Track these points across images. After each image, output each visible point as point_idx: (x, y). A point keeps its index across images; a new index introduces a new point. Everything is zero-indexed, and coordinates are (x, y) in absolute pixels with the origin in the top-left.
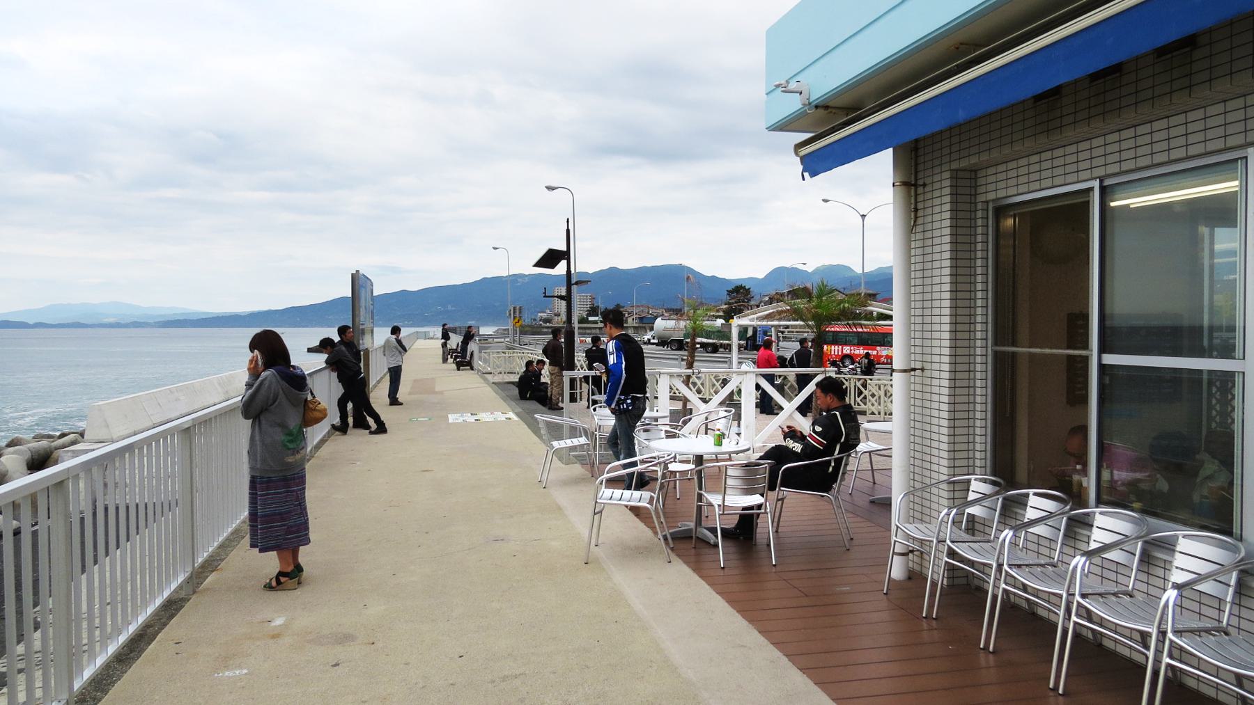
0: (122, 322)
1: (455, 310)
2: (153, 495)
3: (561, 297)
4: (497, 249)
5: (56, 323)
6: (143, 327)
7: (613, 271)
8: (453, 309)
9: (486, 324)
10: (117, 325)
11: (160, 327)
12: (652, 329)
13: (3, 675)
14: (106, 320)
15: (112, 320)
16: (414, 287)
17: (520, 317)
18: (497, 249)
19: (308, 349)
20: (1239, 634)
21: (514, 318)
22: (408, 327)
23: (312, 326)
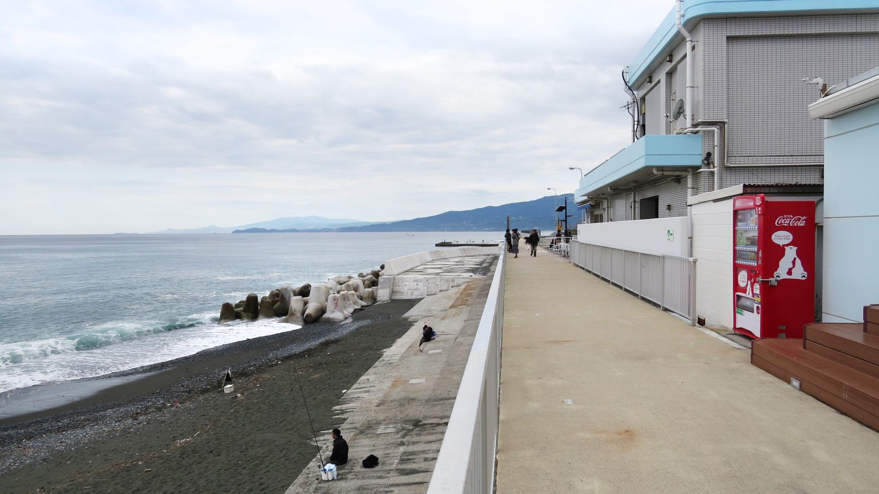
0: (318, 228)
1: (525, 220)
2: (327, 344)
3: (564, 220)
4: (573, 169)
5: (282, 229)
6: (329, 232)
7: (490, 208)
8: (524, 218)
9: (546, 229)
10: (315, 231)
11: (339, 231)
12: (663, 174)
13: (163, 493)
14: (308, 228)
15: (312, 227)
16: (497, 203)
17: (561, 225)
18: (573, 169)
19: (436, 244)
20: (805, 348)
21: (558, 225)
22: (492, 231)
23: (431, 231)
